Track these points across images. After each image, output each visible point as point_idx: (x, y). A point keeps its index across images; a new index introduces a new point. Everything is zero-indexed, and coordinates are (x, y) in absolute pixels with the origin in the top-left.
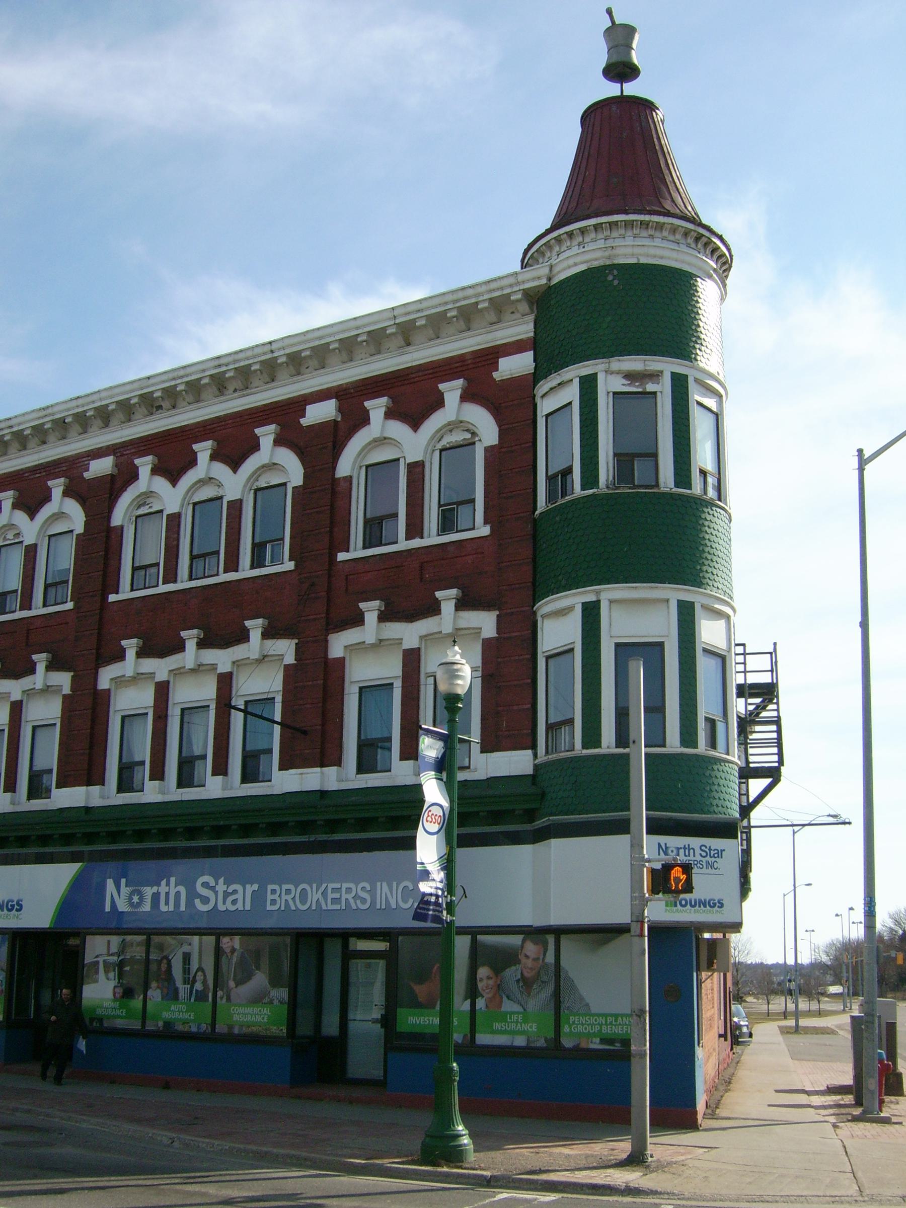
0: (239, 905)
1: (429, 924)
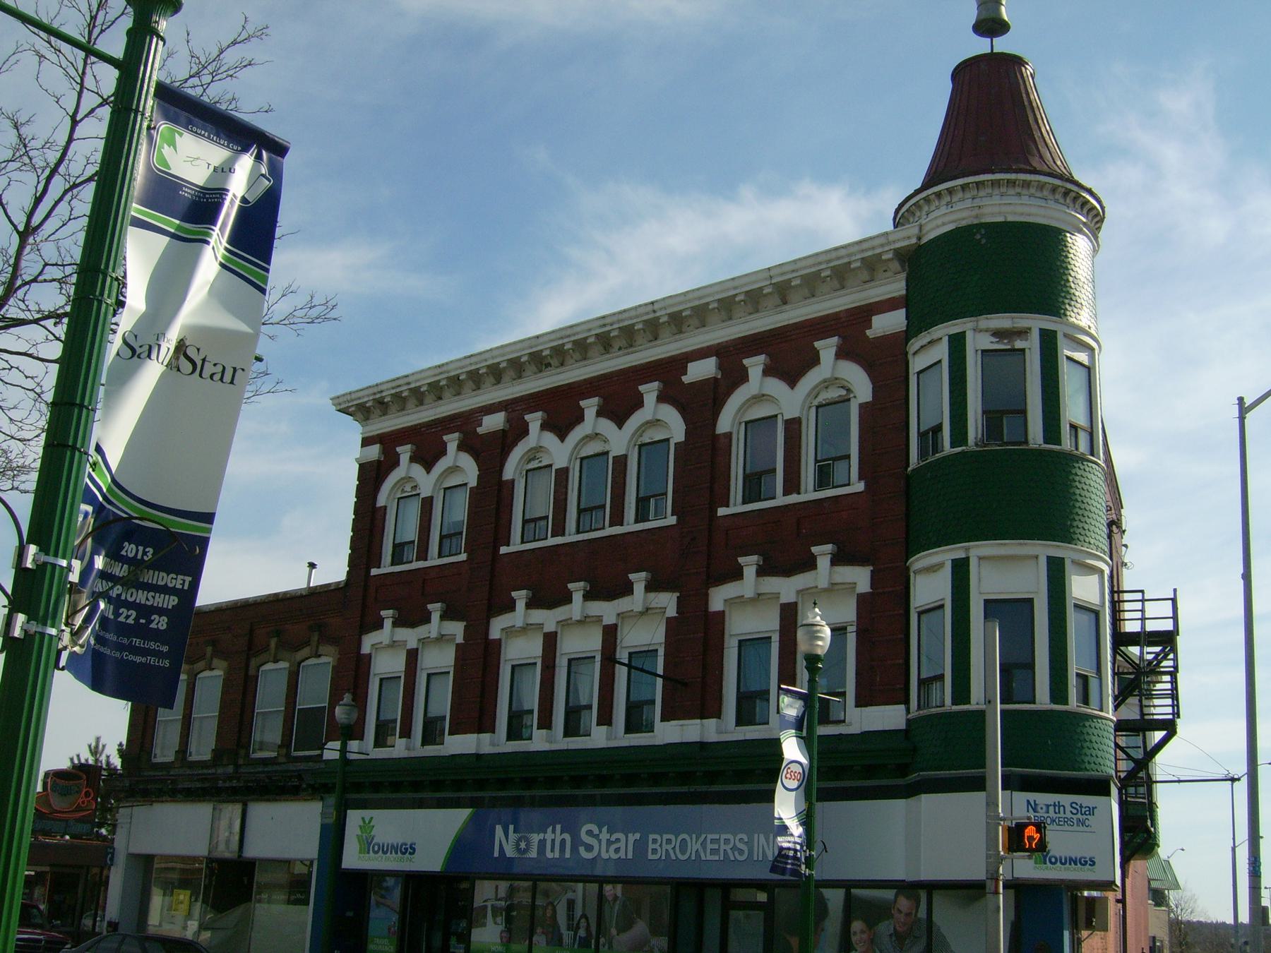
0: (622, 854)
1: (787, 877)
